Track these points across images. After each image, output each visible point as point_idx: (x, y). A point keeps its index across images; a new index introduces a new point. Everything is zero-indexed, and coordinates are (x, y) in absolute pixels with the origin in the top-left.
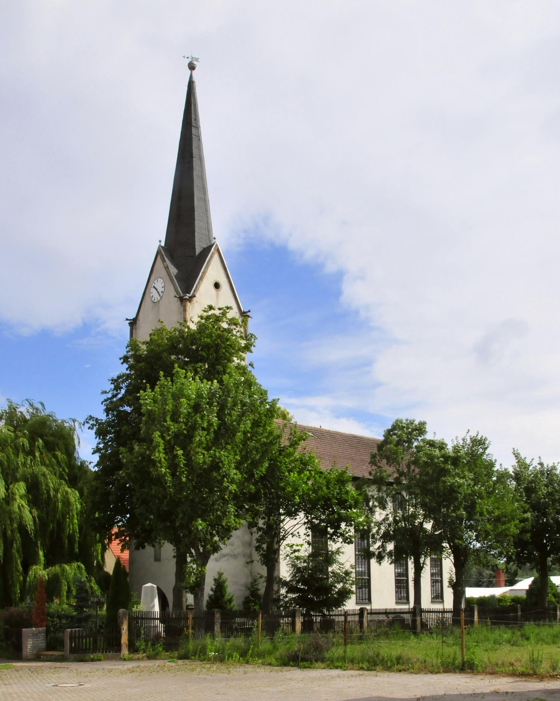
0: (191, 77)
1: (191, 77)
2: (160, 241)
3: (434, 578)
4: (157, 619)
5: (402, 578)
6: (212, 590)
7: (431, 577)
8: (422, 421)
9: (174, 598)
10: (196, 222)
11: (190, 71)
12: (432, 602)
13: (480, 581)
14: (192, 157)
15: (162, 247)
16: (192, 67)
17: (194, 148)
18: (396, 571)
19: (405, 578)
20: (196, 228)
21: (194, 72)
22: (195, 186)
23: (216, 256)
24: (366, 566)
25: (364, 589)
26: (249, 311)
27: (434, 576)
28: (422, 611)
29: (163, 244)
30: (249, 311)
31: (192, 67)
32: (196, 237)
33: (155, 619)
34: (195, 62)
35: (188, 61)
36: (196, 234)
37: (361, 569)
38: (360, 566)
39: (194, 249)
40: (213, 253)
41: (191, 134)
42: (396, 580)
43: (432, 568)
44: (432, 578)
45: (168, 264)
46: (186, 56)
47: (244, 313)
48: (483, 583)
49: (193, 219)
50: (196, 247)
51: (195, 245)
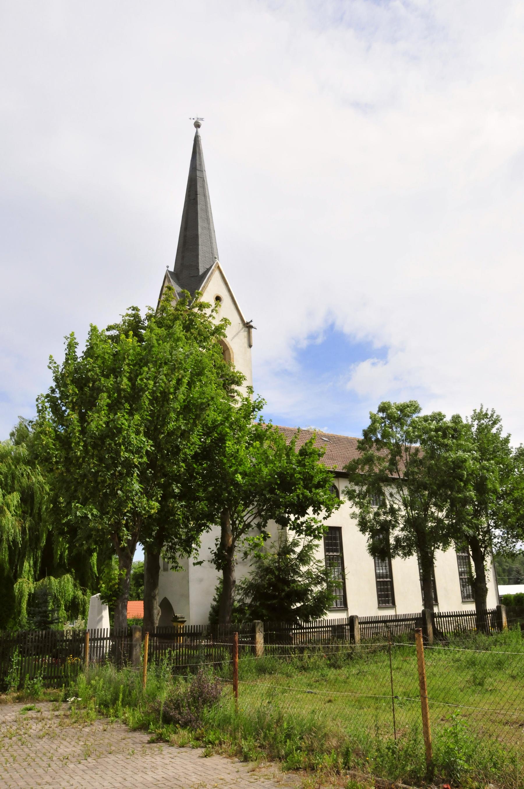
0: (197, 132)
1: (197, 132)
2: (168, 267)
3: (463, 577)
4: (107, 639)
5: (385, 580)
6: (215, 600)
7: (460, 576)
8: (139, 308)
9: (144, 612)
10: (200, 247)
11: (196, 129)
12: (463, 602)
13: (518, 579)
14: (197, 194)
15: (169, 272)
16: (197, 125)
17: (198, 187)
18: (460, 570)
19: (389, 580)
20: (200, 251)
21: (199, 130)
22: (199, 217)
23: (217, 273)
24: (388, 567)
25: (467, 587)
26: (251, 321)
27: (463, 574)
28: (433, 615)
29: (172, 269)
30: (251, 321)
31: (197, 125)
32: (200, 260)
33: (104, 639)
34: (200, 121)
35: (194, 121)
36: (200, 257)
37: (382, 571)
38: (462, 567)
39: (198, 269)
40: (213, 270)
41: (196, 176)
42: (377, 582)
43: (460, 567)
44: (461, 577)
45: (173, 284)
46: (192, 118)
47: (248, 323)
48: (521, 580)
49: (197, 245)
50: (200, 268)
51: (198, 266)
